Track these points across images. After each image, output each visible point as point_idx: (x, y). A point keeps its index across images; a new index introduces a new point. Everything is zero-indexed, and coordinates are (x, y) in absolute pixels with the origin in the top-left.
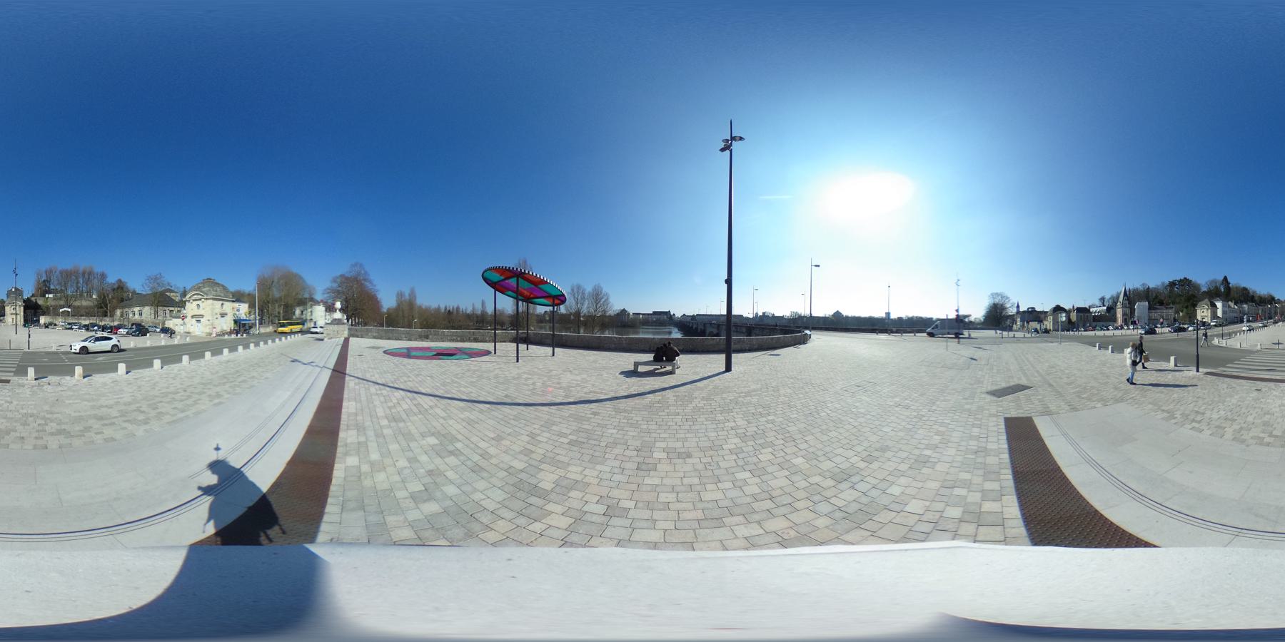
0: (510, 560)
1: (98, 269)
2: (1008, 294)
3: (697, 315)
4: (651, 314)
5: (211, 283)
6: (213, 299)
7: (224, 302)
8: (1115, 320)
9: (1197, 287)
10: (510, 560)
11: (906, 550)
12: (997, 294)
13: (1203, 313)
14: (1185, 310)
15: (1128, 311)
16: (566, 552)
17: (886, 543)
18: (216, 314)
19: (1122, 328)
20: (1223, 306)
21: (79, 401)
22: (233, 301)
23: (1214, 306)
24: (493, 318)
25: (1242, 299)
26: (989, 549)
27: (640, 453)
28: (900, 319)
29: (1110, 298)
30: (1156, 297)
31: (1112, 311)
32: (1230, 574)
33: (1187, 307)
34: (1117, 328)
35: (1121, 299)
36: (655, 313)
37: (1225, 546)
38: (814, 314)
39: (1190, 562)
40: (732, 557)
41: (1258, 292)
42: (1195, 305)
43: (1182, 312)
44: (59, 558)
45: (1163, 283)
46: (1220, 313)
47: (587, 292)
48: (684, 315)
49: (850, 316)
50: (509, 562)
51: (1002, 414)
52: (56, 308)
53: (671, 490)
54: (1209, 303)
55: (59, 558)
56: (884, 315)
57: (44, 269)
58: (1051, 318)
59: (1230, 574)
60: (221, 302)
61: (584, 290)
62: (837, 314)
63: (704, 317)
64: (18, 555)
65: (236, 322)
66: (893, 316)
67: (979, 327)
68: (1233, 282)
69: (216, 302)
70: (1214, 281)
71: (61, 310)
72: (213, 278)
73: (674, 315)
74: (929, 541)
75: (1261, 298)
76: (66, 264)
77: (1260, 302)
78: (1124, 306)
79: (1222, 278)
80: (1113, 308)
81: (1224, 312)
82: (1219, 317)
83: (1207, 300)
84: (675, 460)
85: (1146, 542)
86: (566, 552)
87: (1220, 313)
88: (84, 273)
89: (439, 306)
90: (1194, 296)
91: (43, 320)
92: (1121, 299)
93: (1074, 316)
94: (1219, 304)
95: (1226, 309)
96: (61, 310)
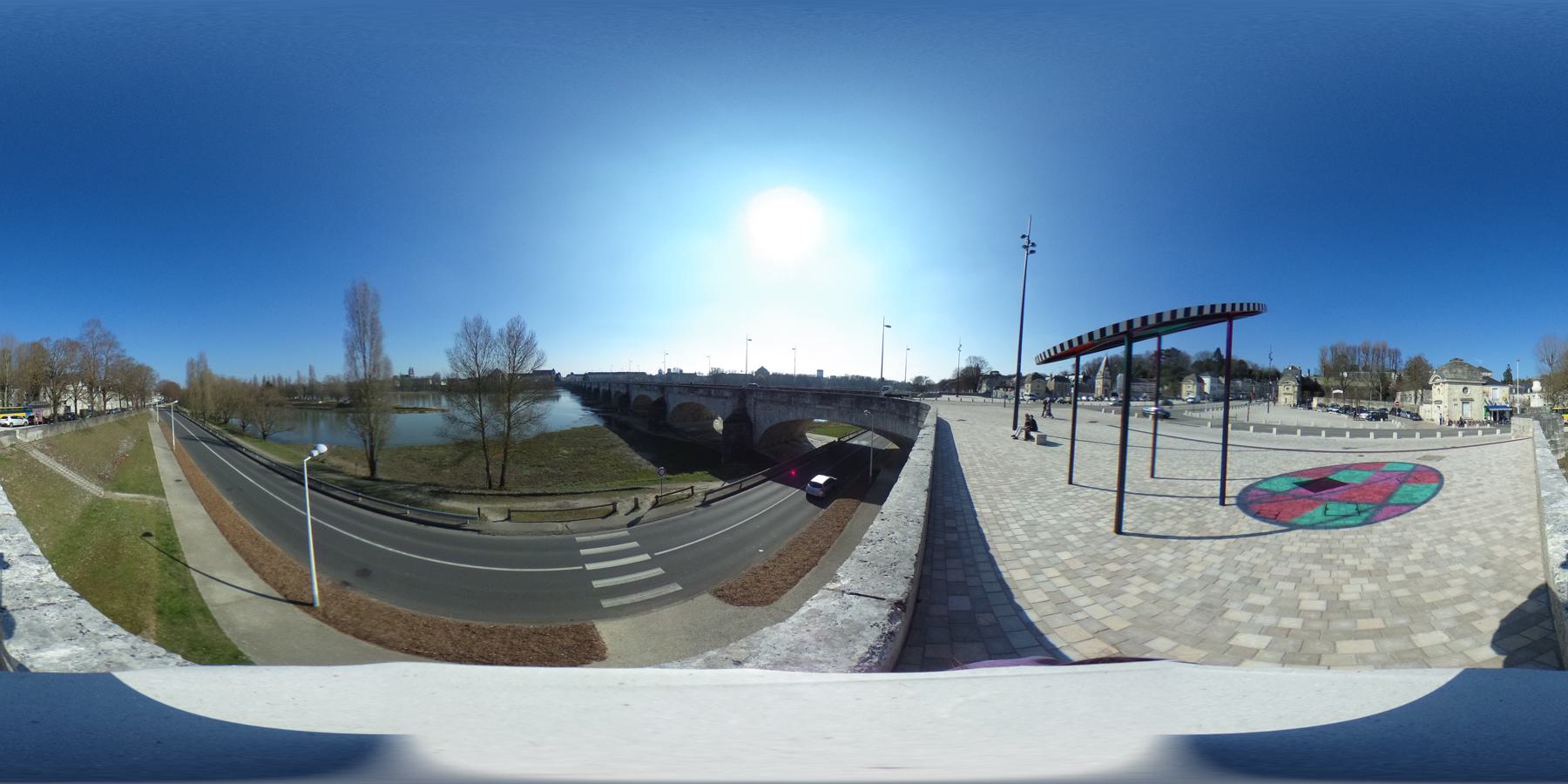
1: (1392, 346)
2: (987, 359)
5: (1457, 363)
6: (1449, 383)
7: (1467, 386)
8: (1092, 389)
9: (1186, 358)
12: (975, 358)
13: (1189, 389)
14: (1170, 383)
15: (1109, 382)
18: (1455, 400)
19: (1102, 400)
20: (1212, 382)
21: (1135, 481)
22: (1484, 384)
23: (1201, 381)
24: (1135, 387)
25: (1238, 373)
28: (833, 378)
29: (1085, 365)
30: (1139, 368)
31: (1089, 380)
32: (1501, 701)
33: (1172, 381)
34: (1096, 400)
35: (1102, 368)
38: (887, 377)
42: (1181, 379)
43: (1167, 385)
45: (1148, 352)
46: (1207, 389)
47: (494, 332)
48: (572, 374)
50: (147, 539)
51: (24, 414)
52: (1329, 390)
53: (512, 514)
54: (1195, 378)
56: (814, 373)
57: (1329, 345)
58: (1030, 385)
60: (1463, 386)
61: (487, 330)
62: (762, 370)
63: (597, 376)
65: (1487, 409)
66: (826, 375)
69: (1455, 386)
70: (1206, 353)
71: (1334, 392)
72: (1461, 358)
73: (559, 374)
75: (1261, 372)
76: (1354, 337)
77: (1261, 378)
78: (1104, 377)
79: (1215, 350)
80: (1090, 378)
81: (1212, 388)
82: (1206, 393)
83: (1193, 375)
84: (994, 531)
87: (1207, 389)
88: (1374, 350)
90: (1182, 369)
91: (1315, 402)
92: (1102, 368)
93: (1051, 385)
94: (1207, 380)
95: (1215, 385)
96: (1334, 392)
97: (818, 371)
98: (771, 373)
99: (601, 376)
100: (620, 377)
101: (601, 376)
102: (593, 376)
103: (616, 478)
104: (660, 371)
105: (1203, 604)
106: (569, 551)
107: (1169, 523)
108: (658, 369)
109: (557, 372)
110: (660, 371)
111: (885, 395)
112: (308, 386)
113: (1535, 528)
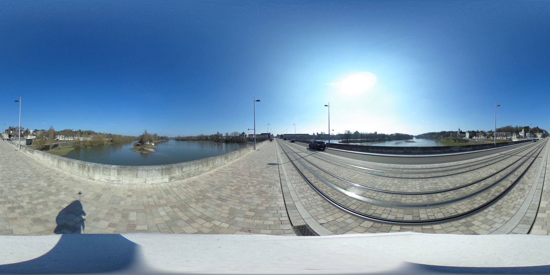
0: (218, 240)
3: (284, 135)
4: (260, 135)
10: (218, 240)
11: (388, 236)
16: (242, 237)
17: (381, 233)
26: (423, 235)
27: (267, 195)
32: (526, 246)
36: (262, 134)
37: (508, 234)
39: (509, 241)
40: (313, 239)
41: (224, 135)
44: (25, 239)
48: (278, 135)
49: (427, 133)
55: (25, 239)
56: (312, 134)
59: (526, 246)
63: (288, 136)
64: (8, 238)
67: (336, 142)
68: (149, 132)
73: (272, 135)
74: (235, 234)
85: (196, 234)
86: (242, 237)
89: (146, 131)
97: (375, 132)
98: (158, 135)
99: (289, 136)
100: (298, 136)
101: (289, 136)
102: (286, 136)
103: (500, 136)
104: (314, 134)
105: (98, 221)
106: (528, 132)
107: (339, 175)
108: (313, 133)
109: (271, 134)
110: (314, 134)
111: (259, 178)
112: (226, 136)
113: (446, 230)
